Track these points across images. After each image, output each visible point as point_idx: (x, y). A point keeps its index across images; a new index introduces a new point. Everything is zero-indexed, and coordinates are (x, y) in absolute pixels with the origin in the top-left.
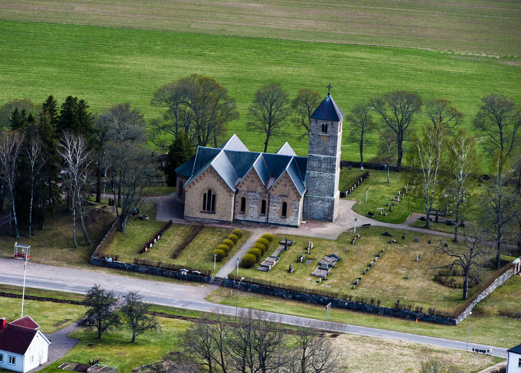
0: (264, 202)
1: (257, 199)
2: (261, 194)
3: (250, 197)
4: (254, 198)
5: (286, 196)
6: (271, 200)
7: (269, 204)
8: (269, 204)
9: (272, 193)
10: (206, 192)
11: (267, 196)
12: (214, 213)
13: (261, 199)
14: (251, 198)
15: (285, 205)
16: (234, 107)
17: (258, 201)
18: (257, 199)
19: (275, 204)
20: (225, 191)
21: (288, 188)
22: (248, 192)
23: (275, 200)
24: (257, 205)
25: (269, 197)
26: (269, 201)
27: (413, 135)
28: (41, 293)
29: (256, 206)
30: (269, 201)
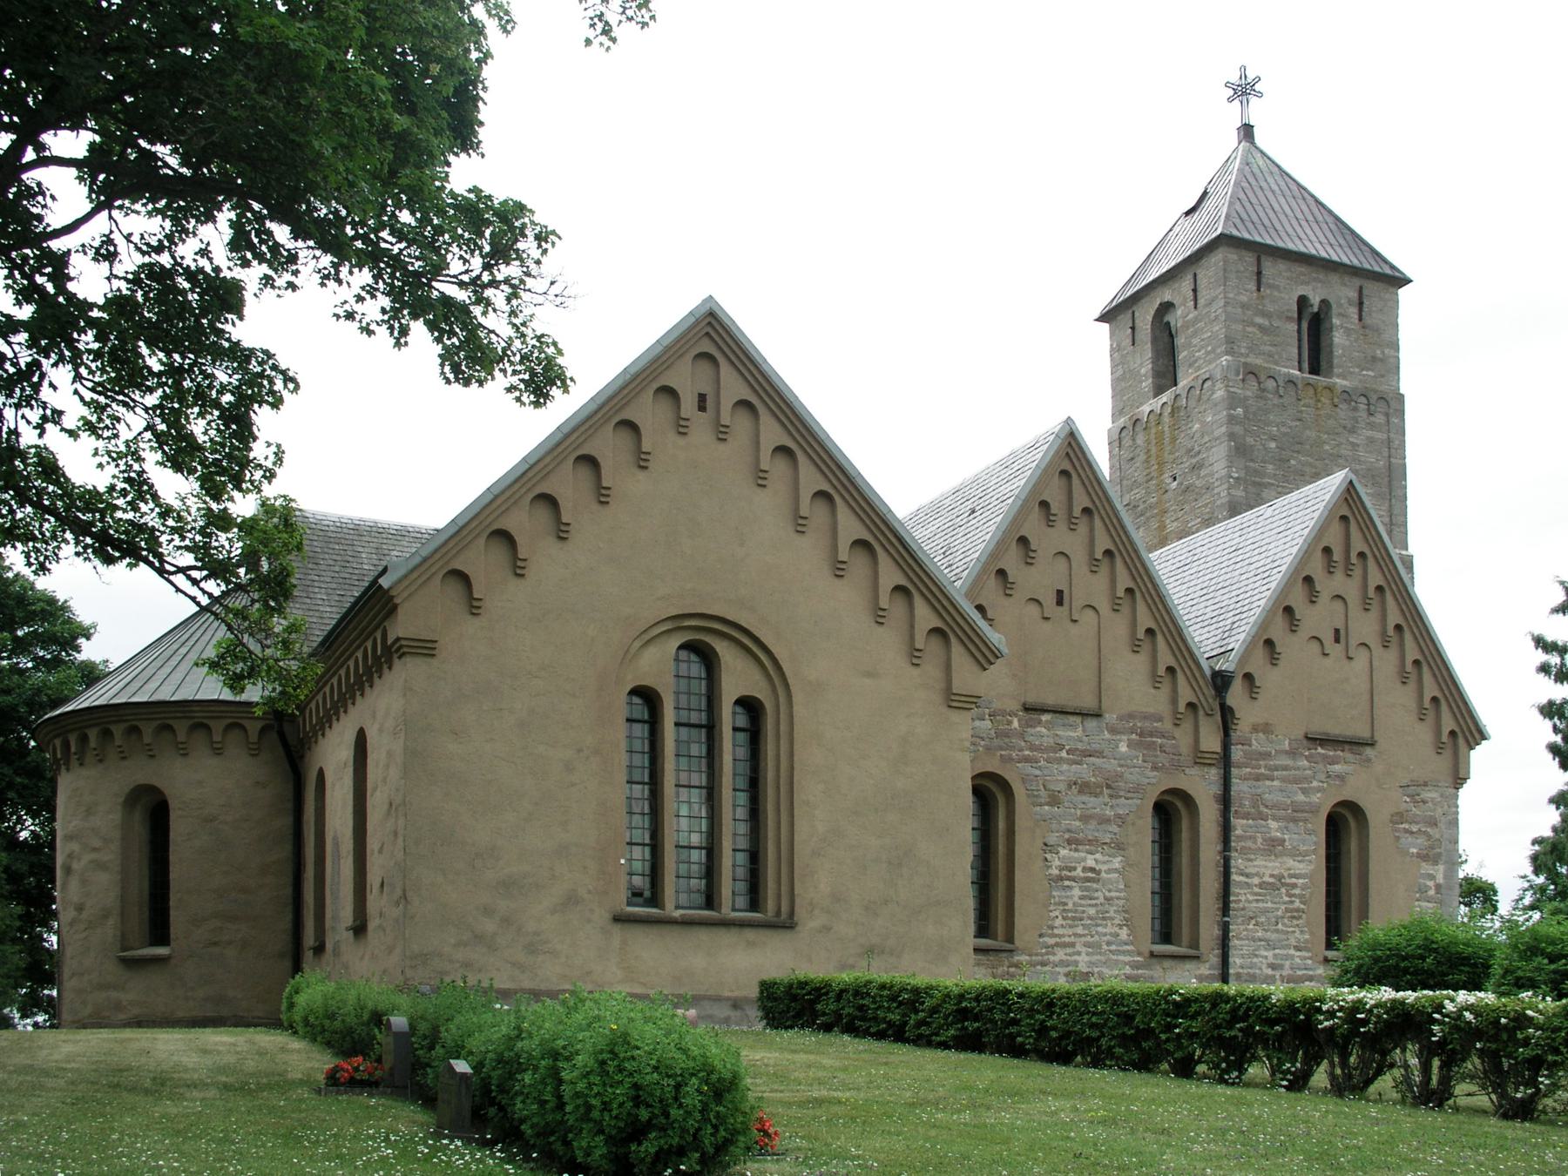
0: (1170, 812)
1: (1110, 785)
2: (1144, 740)
3: (1047, 767)
4: (1083, 771)
6: (1240, 787)
9: (1247, 713)
10: (660, 665)
12: (785, 924)
13: (1157, 784)
14: (1061, 774)
15: (1342, 825)
16: (1250, 1062)
17: (1124, 806)
18: (1110, 785)
20: (888, 641)
21: (1361, 658)
23: (1272, 790)
24: (1120, 847)
25: (1225, 761)
26: (1225, 800)
27: (64, 623)
28: (182, 1097)
29: (1109, 864)
30: (1225, 800)
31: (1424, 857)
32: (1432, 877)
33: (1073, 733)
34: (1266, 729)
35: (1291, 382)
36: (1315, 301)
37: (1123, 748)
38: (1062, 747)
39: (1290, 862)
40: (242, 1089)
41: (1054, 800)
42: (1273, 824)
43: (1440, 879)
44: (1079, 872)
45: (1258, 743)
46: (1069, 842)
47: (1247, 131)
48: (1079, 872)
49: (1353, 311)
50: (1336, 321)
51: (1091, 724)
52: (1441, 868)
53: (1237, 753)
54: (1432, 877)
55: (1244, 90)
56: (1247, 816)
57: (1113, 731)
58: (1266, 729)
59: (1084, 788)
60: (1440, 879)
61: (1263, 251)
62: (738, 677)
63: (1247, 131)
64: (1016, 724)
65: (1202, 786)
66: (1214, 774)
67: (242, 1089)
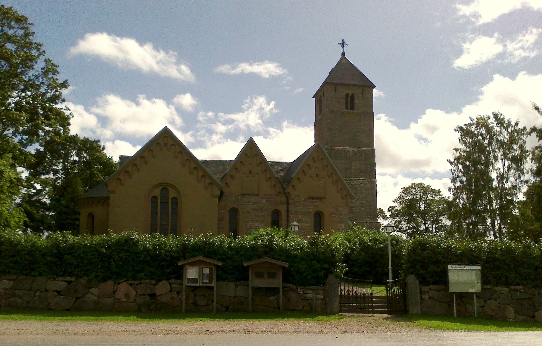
5: (321, 199)
6: (291, 208)
7: (288, 217)
8: (288, 217)
10: (157, 192)
11: (284, 199)
19: (300, 217)
22: (243, 195)
24: (263, 221)
25: (288, 203)
26: (288, 211)
30: (288, 211)
31: (339, 222)
32: (341, 227)
33: (253, 199)
34: (298, 196)
35: (343, 113)
36: (350, 94)
37: (264, 201)
38: (249, 202)
39: (304, 224)
40: (51, 309)
41: (248, 212)
42: (300, 216)
43: (343, 227)
44: (254, 227)
45: (296, 199)
46: (252, 221)
47: (343, 54)
48: (254, 227)
49: (361, 95)
50: (356, 98)
51: (257, 197)
52: (343, 225)
53: (291, 201)
54: (341, 227)
55: (343, 45)
56: (293, 214)
57: (262, 198)
58: (298, 196)
59: (255, 210)
60: (343, 227)
61: (336, 85)
62: (172, 194)
63: (343, 54)
64: (240, 198)
65: (282, 209)
66: (285, 206)
67: (51, 309)
